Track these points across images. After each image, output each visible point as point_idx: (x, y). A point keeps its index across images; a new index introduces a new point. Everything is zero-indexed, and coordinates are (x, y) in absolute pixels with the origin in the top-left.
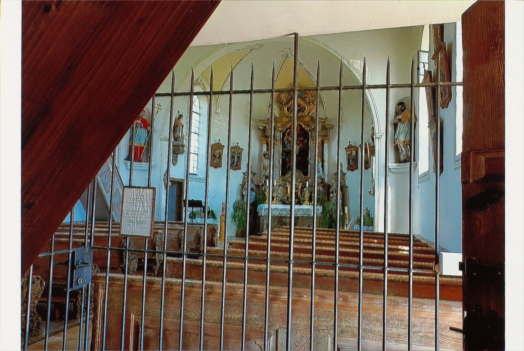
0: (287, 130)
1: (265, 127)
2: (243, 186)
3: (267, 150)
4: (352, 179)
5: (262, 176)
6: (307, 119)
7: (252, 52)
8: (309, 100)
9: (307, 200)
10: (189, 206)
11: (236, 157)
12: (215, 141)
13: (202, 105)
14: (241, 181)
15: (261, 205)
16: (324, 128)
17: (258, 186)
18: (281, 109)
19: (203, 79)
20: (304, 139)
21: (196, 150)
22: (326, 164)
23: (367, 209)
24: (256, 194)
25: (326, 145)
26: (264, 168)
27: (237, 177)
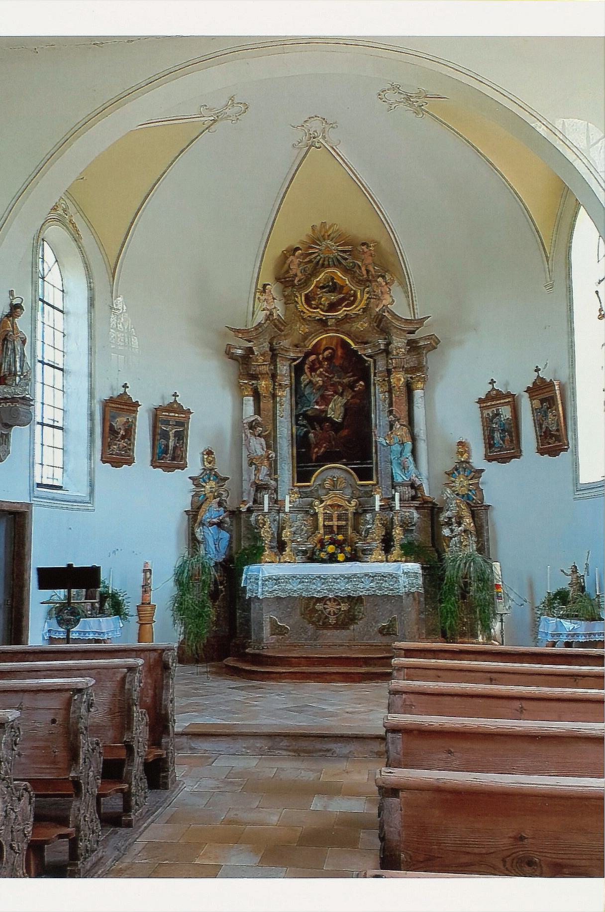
0: (307, 355)
1: (250, 350)
2: (193, 515)
3: (258, 411)
4: (499, 483)
5: (246, 486)
6: (361, 325)
7: (217, 125)
8: (368, 271)
9: (377, 544)
10: (42, 585)
11: (171, 434)
12: (112, 388)
13: (70, 286)
14: (185, 502)
15: (253, 567)
16: (413, 346)
17: (234, 514)
18: (288, 300)
19: (72, 209)
20: (357, 381)
21: (59, 415)
22: (422, 447)
23: (575, 570)
24: (231, 537)
25: (418, 394)
26: (251, 464)
27: (174, 491)
